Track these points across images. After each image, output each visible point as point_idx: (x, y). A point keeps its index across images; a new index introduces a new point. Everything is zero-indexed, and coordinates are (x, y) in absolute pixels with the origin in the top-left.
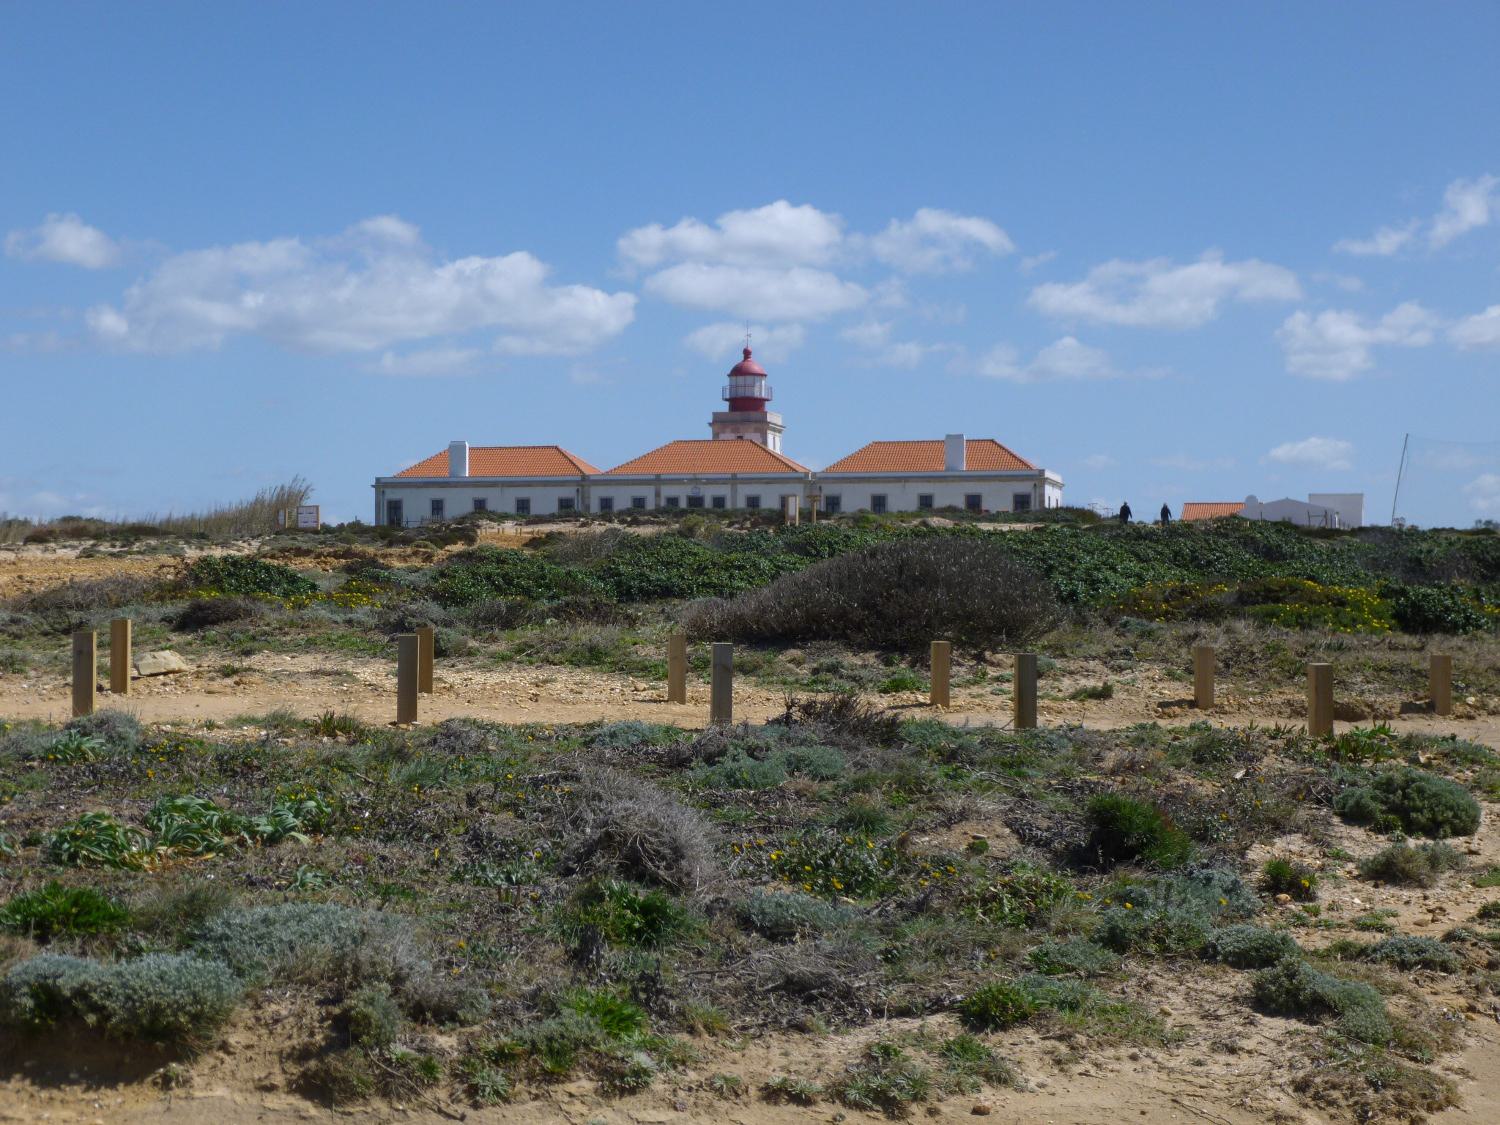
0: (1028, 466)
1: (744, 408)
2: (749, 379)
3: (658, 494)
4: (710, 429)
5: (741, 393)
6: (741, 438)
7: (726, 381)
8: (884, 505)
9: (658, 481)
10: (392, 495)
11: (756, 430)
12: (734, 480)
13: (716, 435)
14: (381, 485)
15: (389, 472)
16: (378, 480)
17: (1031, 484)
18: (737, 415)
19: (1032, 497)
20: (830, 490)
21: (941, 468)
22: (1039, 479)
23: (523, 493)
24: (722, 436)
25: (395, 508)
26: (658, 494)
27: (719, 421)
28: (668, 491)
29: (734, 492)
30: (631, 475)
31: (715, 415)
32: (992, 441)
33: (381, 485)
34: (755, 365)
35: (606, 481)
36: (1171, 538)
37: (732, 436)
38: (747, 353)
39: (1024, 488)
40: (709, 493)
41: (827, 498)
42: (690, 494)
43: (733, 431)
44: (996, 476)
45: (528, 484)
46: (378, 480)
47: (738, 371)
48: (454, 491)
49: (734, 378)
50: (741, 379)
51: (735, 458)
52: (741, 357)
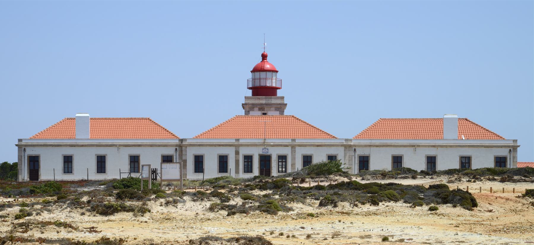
1: (263, 92)
3: (237, 153)
7: (250, 76)
26: (237, 153)
28: (244, 151)
37: (259, 113)
38: (264, 57)
42: (261, 153)
52: (261, 59)
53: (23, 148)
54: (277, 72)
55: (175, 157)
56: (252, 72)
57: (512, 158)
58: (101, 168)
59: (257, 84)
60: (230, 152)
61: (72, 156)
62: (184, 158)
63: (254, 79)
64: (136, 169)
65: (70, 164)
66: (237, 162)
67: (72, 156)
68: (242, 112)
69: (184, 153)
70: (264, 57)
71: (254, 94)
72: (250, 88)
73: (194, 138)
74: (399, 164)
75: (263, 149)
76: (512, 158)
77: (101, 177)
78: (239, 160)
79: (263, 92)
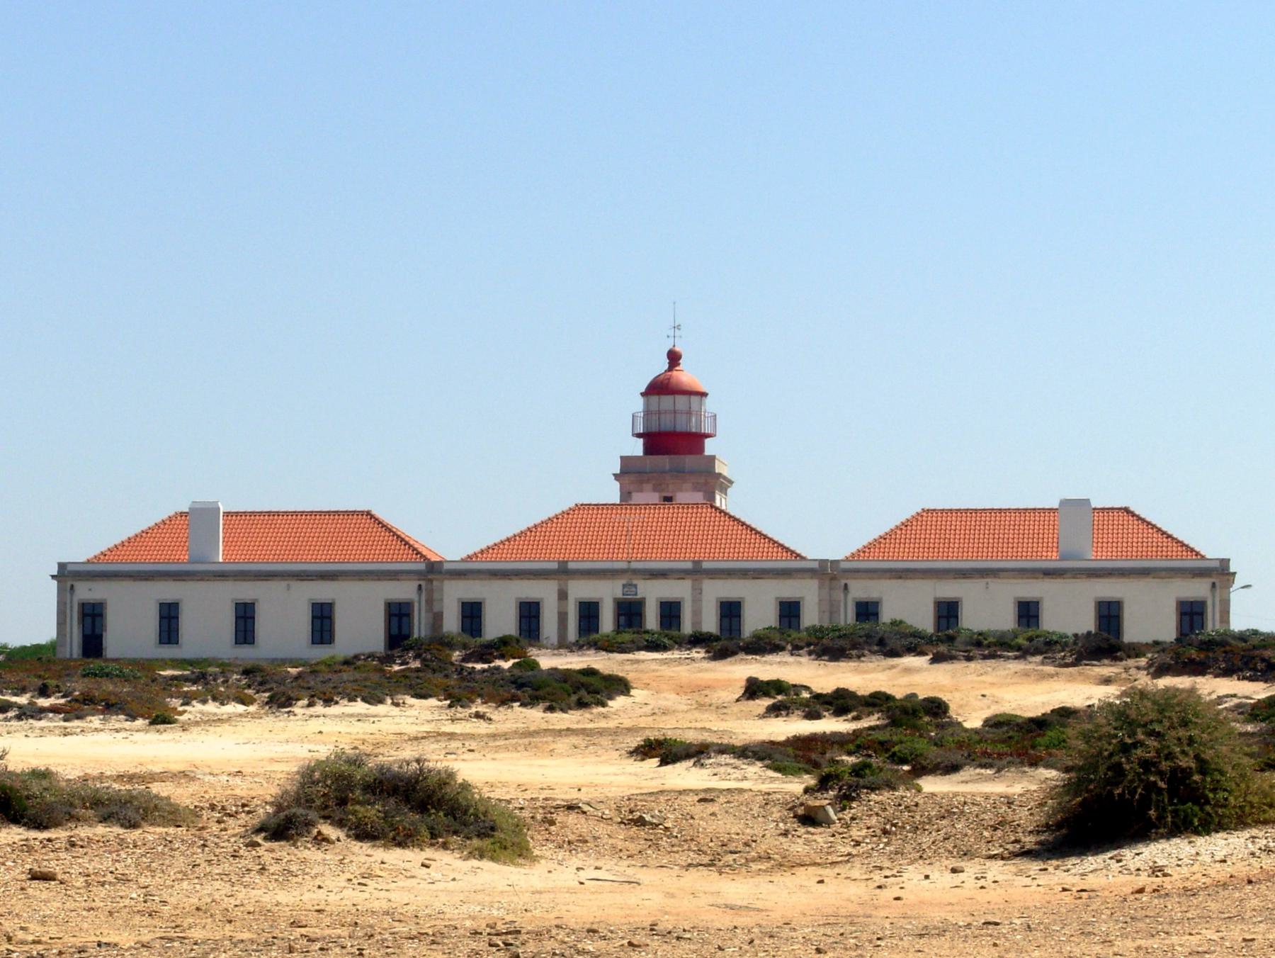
0: (1197, 554)
1: (671, 445)
2: (681, 400)
3: (563, 595)
4: (617, 485)
5: (667, 424)
6: (668, 499)
7: (638, 405)
8: (798, 616)
9: (563, 572)
10: (87, 592)
11: (696, 488)
12: (697, 572)
13: (626, 495)
14: (67, 576)
15: (80, 552)
16: (62, 566)
17: (414, 584)
18: (664, 461)
19: (1209, 603)
20: (861, 590)
21: (1051, 559)
22: (1221, 573)
23: (323, 591)
24: (637, 498)
25: (91, 621)
26: (563, 595)
27: (629, 472)
28: (581, 590)
29: (697, 593)
30: (147, 560)
31: (624, 460)
32: (1127, 510)
33: (67, 576)
34: (687, 374)
35: (460, 574)
36: (769, 683)
37: (654, 497)
38: (674, 358)
39: (1196, 590)
40: (653, 594)
41: (83, 606)
42: (619, 595)
43: (655, 490)
44: (890, 571)
45: (744, 574)
46: (62, 566)
47: (659, 388)
48: (277, 586)
49: (654, 399)
50: (667, 401)
51: (664, 536)
52: (664, 364)
53: (69, 584)
54: (704, 395)
55: (416, 605)
56: (642, 394)
57: (1217, 603)
58: (730, 630)
59: (654, 429)
60: (544, 592)
61: (538, 604)
62: (436, 609)
63: (648, 413)
64: (326, 635)
65: (735, 620)
66: (562, 618)
67: (538, 604)
68: (612, 493)
69: (436, 596)
70: (674, 358)
71: (649, 450)
72: (639, 436)
73: (462, 560)
74: (793, 620)
75: (624, 586)
76: (1217, 603)
77: (321, 653)
78: (566, 614)
79: (671, 445)
